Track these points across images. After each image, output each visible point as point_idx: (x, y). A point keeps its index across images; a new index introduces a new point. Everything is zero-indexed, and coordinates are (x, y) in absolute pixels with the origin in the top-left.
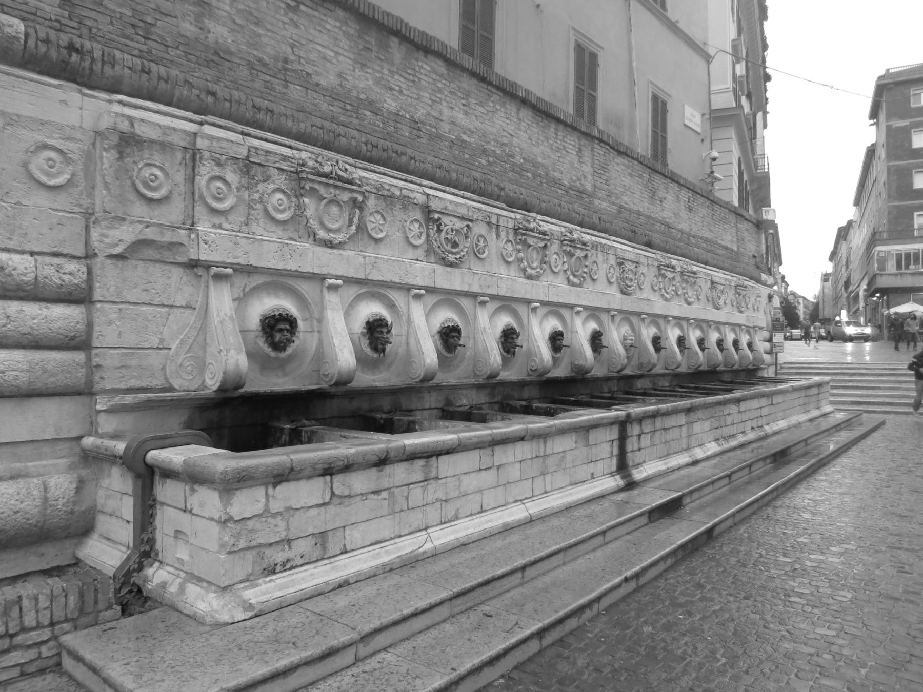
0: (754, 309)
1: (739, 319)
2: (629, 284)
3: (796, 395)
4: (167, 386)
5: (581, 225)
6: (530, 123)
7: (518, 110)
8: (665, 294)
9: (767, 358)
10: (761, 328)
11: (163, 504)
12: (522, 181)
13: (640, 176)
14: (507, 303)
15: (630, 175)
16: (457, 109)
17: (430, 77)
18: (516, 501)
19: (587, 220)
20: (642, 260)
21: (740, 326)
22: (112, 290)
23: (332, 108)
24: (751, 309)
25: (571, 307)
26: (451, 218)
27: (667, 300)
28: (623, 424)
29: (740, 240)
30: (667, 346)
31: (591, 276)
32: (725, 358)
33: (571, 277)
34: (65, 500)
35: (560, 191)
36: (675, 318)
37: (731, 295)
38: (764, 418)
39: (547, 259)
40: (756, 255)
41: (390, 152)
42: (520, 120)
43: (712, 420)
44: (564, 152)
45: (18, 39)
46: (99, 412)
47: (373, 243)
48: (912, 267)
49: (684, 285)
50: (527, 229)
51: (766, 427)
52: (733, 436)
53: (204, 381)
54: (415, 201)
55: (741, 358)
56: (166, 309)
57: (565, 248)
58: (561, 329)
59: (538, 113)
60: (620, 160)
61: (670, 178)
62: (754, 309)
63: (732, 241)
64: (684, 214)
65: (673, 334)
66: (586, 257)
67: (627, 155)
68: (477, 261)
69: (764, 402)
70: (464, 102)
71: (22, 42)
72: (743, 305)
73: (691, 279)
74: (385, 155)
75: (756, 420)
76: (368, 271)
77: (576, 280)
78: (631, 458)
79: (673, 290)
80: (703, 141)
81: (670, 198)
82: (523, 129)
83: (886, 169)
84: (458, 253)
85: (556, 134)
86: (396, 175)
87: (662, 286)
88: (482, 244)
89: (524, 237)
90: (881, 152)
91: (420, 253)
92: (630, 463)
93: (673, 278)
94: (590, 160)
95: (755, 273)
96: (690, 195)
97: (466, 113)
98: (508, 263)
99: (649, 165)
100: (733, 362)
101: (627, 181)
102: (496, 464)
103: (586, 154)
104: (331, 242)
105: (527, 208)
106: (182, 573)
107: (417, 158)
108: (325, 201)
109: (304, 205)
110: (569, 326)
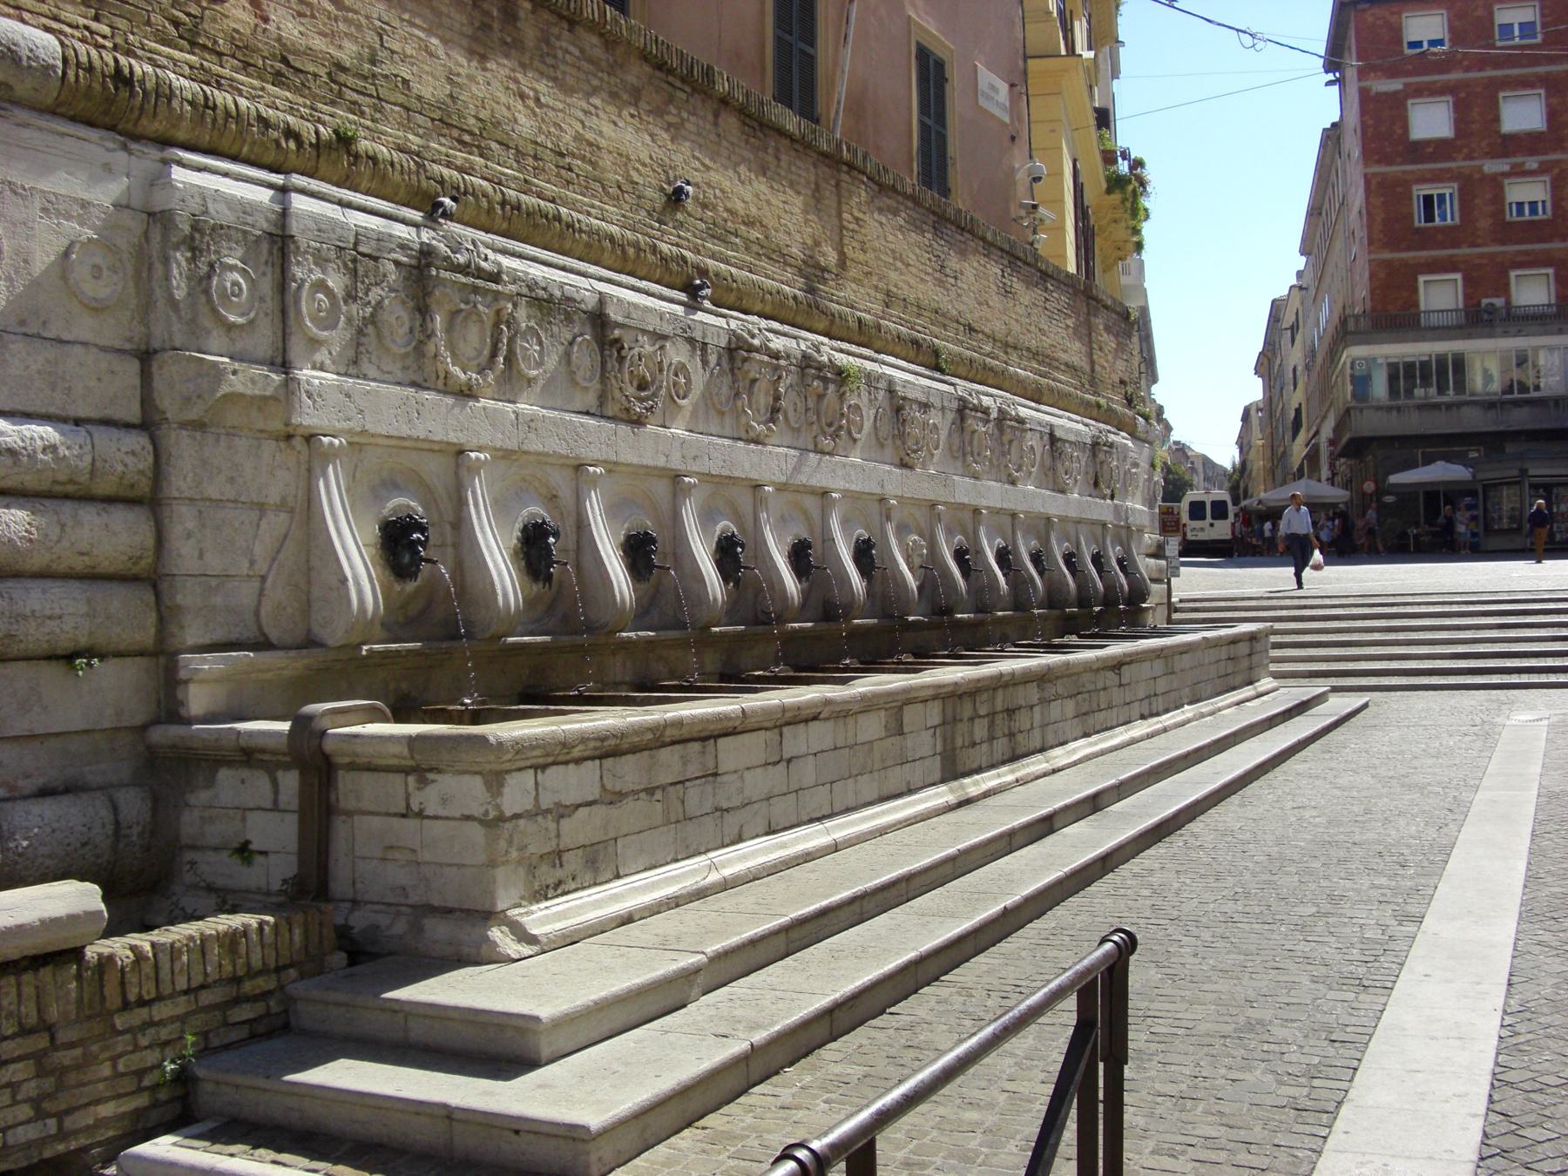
4: (262, 639)
11: (350, 814)
22: (189, 479)
34: (140, 828)
38: (1160, 698)
40: (1126, 379)
41: (538, 217)
42: (719, 136)
45: (54, 67)
48: (1419, 392)
59: (747, 121)
64: (996, 301)
71: (60, 72)
76: (522, 436)
80: (1013, 138)
83: (1362, 183)
85: (778, 159)
90: (1352, 145)
96: (1006, 262)
102: (786, 756)
106: (403, 909)
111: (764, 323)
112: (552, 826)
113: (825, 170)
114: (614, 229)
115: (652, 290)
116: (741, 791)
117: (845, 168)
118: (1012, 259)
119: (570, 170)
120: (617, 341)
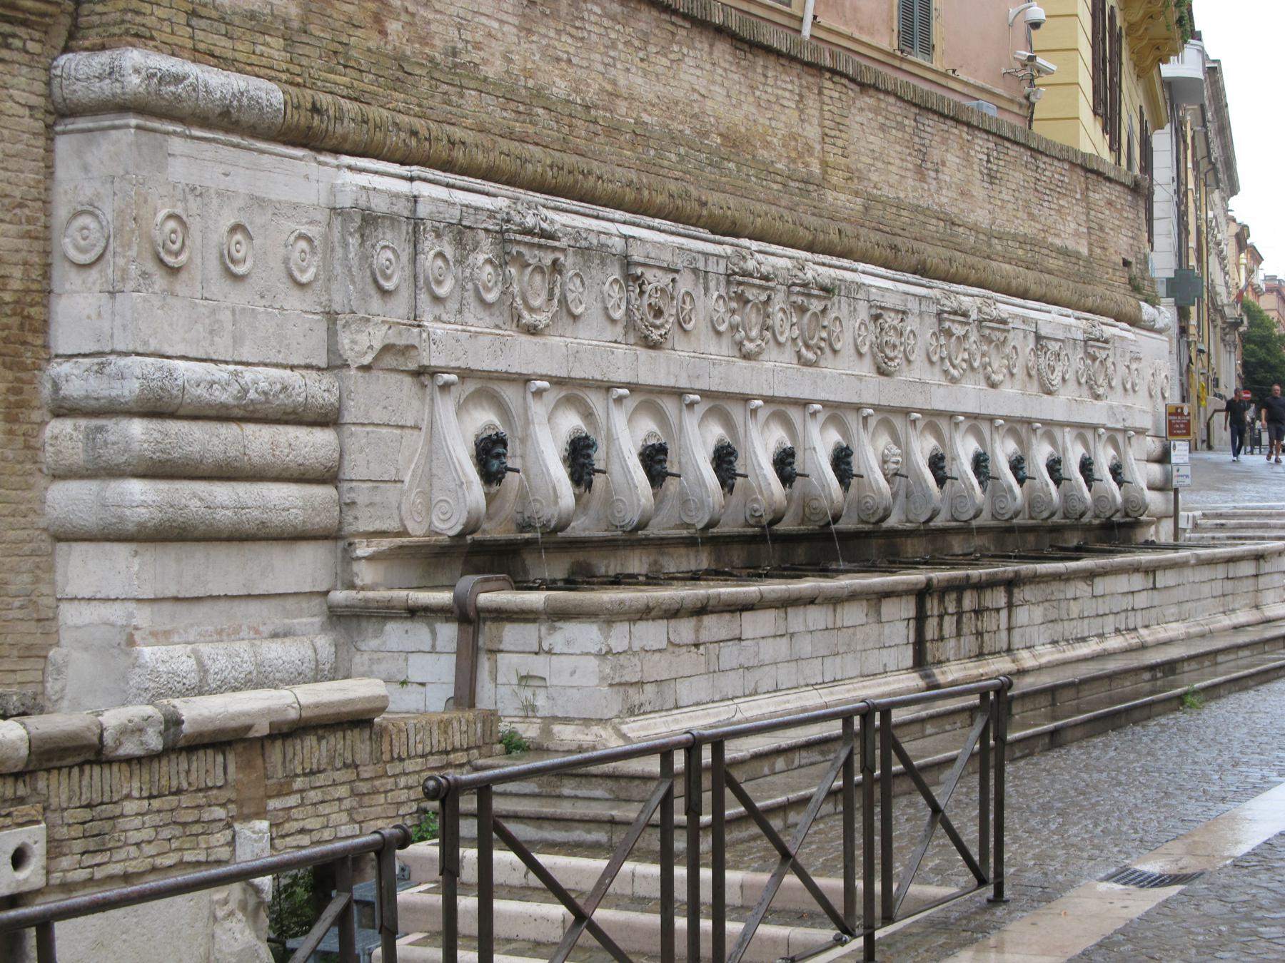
0: (1125, 390)
1: (1095, 413)
2: (891, 355)
3: (1206, 573)
5: (810, 248)
6: (727, 66)
7: (711, 46)
8: (952, 370)
9: (1155, 501)
10: (1141, 432)
12: (724, 179)
13: (900, 126)
14: (717, 403)
15: (882, 127)
16: (634, 70)
17: (601, 26)
18: (807, 685)
19: (821, 237)
20: (913, 305)
21: (1095, 428)
23: (505, 114)
24: (1119, 389)
25: (803, 404)
26: (655, 271)
27: (953, 380)
28: (922, 594)
29: (1095, 231)
30: (863, 472)
31: (831, 346)
32: (1066, 498)
33: (804, 350)
35: (775, 186)
36: (968, 416)
37: (1076, 360)
38: (1139, 613)
39: (770, 322)
41: (576, 173)
42: (714, 64)
43: (1047, 604)
44: (777, 108)
46: (359, 559)
47: (571, 321)
49: (985, 348)
50: (745, 273)
51: (1143, 632)
52: (1083, 639)
53: (431, 523)
54: (613, 251)
55: (1098, 499)
56: (398, 431)
57: (794, 298)
58: (728, 440)
59: (739, 45)
60: (867, 100)
61: (952, 119)
62: (1125, 390)
63: (1077, 234)
64: (979, 190)
65: (965, 449)
66: (824, 311)
67: (877, 89)
68: (682, 335)
69: (1138, 581)
70: (641, 54)
72: (1100, 381)
73: (998, 334)
74: (571, 179)
75: (1123, 615)
77: (810, 355)
78: (932, 651)
79: (964, 360)
81: (952, 159)
82: (719, 79)
84: (662, 326)
85: (766, 76)
86: (588, 211)
87: (945, 354)
88: (688, 307)
89: (741, 288)
91: (619, 331)
92: (929, 658)
93: (965, 336)
94: (817, 113)
95: (1128, 302)
96: (991, 145)
97: (645, 74)
98: (718, 333)
99: (916, 101)
100: (1080, 507)
101: (876, 141)
103: (811, 103)
104: (535, 327)
105: (734, 231)
107: (605, 177)
108: (530, 269)
109: (511, 278)
110: (801, 439)
111: (755, 245)
112: (638, 663)
113: (808, 79)
114: (633, 175)
115: (663, 227)
116: (757, 654)
117: (828, 75)
118: (999, 141)
119: (596, 122)
120: (638, 278)
